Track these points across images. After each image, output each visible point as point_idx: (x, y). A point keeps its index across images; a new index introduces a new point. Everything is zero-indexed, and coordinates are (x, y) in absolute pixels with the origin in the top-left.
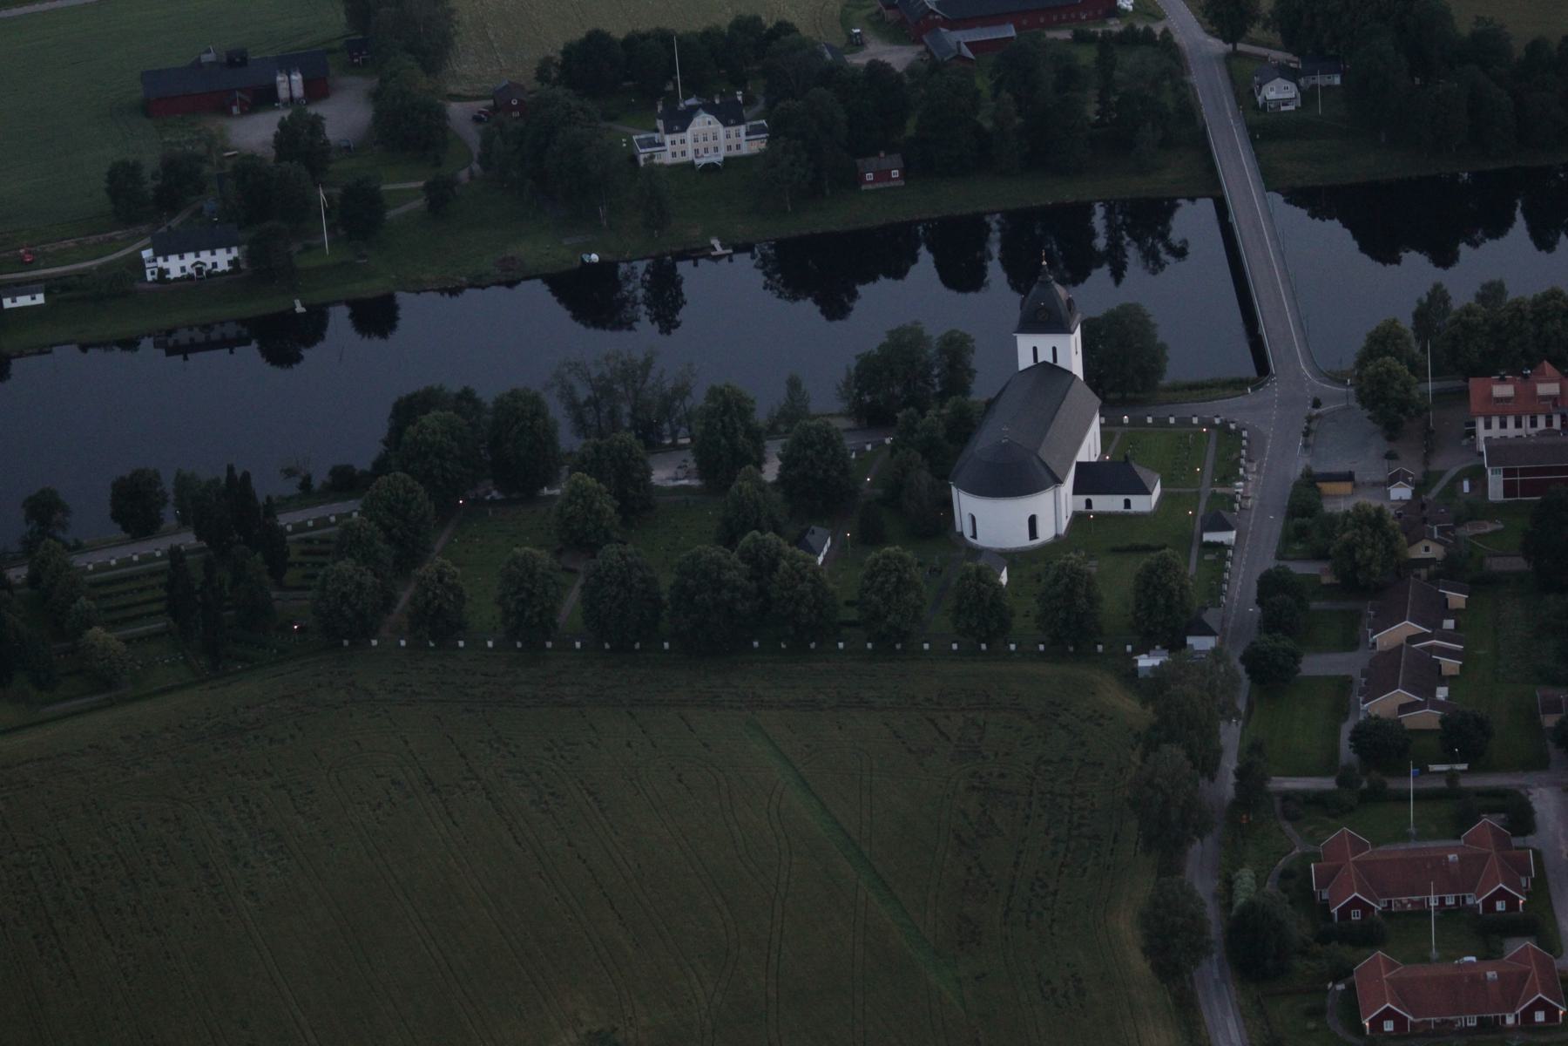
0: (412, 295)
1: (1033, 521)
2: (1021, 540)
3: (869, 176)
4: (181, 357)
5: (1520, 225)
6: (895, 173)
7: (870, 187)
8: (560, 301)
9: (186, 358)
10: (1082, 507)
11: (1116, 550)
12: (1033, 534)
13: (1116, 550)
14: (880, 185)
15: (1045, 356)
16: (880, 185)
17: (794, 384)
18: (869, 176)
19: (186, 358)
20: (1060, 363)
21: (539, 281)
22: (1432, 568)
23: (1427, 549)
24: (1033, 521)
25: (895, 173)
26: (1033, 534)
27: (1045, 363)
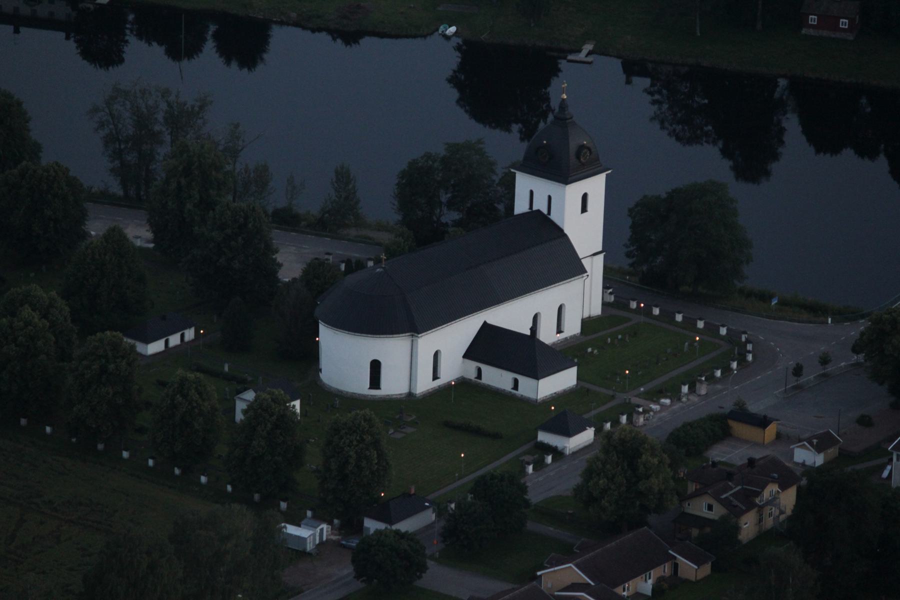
0: (308, 33)
1: (376, 367)
2: (360, 385)
3: (813, 19)
4: (10, 29)
5: (210, 46)
6: (844, 23)
7: (812, 32)
8: (804, 132)
9: (17, 31)
10: (472, 375)
11: (447, 424)
12: (375, 382)
13: (447, 424)
14: (825, 33)
15: (540, 205)
16: (825, 33)
17: (343, 178)
18: (813, 19)
19: (17, 31)
20: (554, 217)
21: (324, 33)
22: (708, 530)
23: (710, 508)
24: (376, 367)
25: (844, 23)
26: (375, 382)
27: (539, 211)
